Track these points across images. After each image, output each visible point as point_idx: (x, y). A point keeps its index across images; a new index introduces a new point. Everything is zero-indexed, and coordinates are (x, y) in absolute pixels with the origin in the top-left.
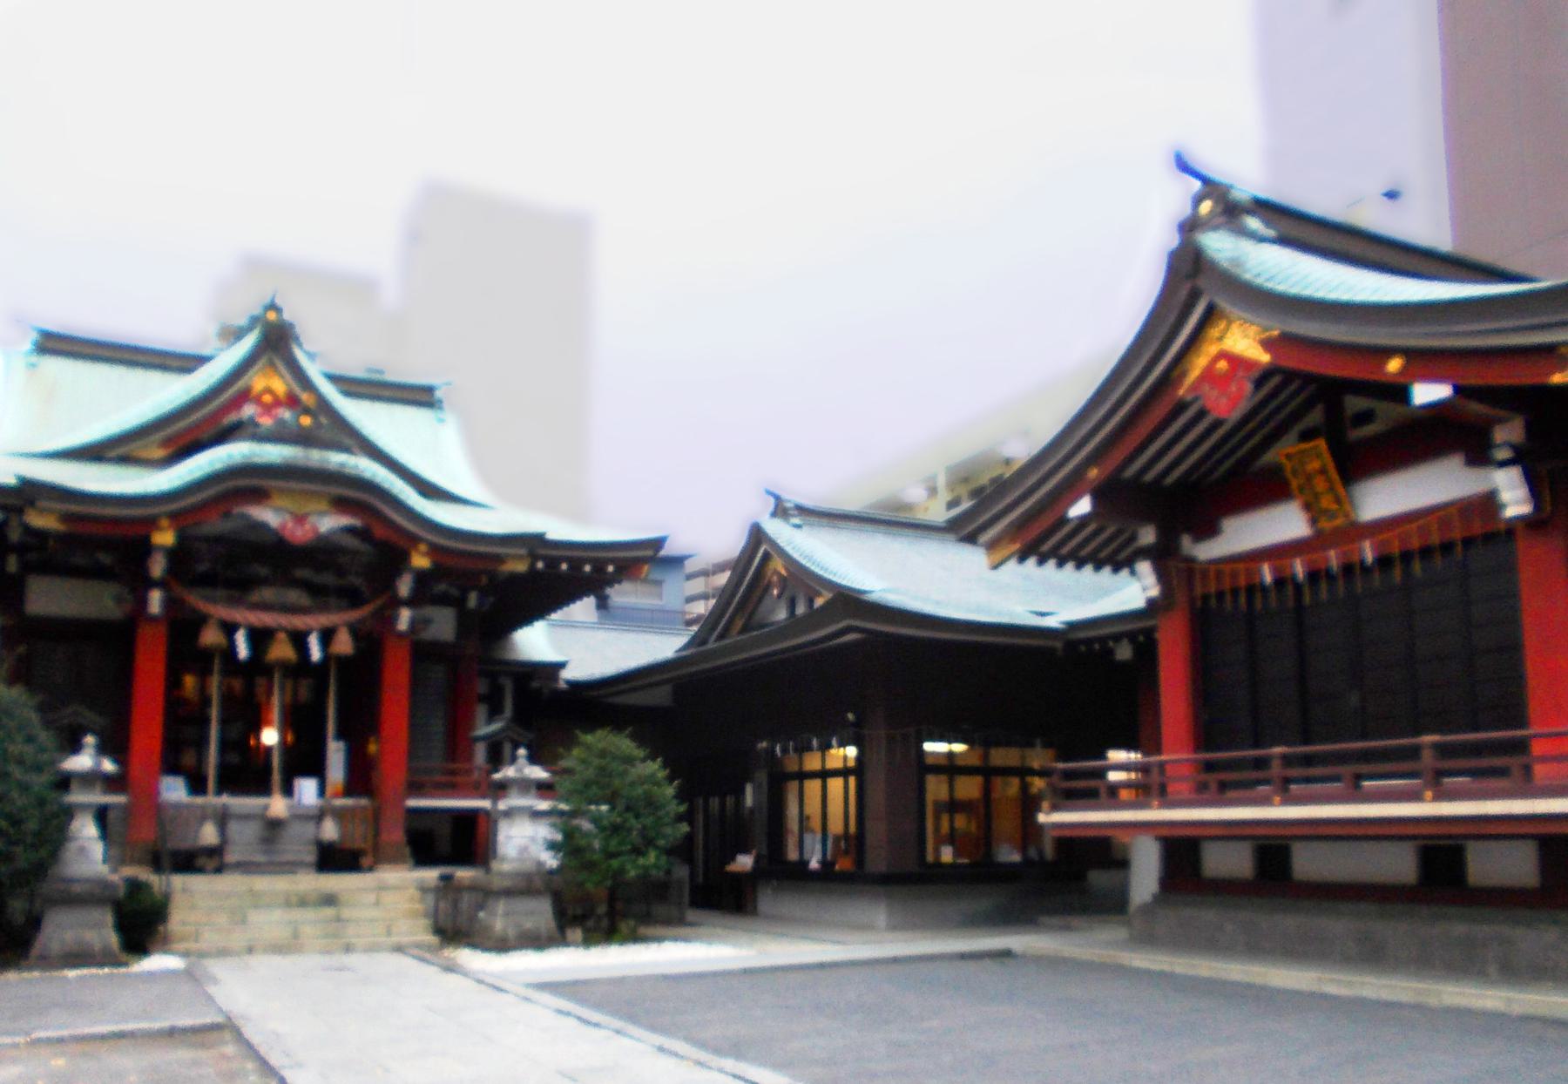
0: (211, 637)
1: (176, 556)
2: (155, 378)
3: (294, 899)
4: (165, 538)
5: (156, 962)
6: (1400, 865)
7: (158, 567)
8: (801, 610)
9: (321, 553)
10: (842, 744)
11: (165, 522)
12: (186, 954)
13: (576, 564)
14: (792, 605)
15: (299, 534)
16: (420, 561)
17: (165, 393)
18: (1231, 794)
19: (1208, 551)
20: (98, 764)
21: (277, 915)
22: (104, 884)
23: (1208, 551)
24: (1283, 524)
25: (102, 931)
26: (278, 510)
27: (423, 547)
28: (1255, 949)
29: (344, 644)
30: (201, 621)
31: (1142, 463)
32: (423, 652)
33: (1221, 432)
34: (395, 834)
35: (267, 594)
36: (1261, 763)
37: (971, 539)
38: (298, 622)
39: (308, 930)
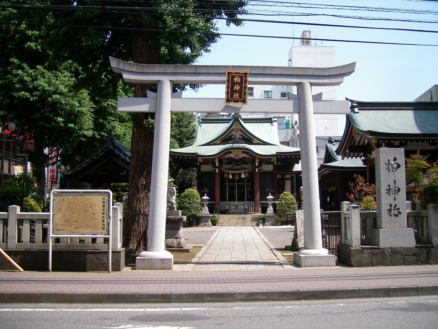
0: (226, 176)
29: (247, 175)
38: (239, 172)
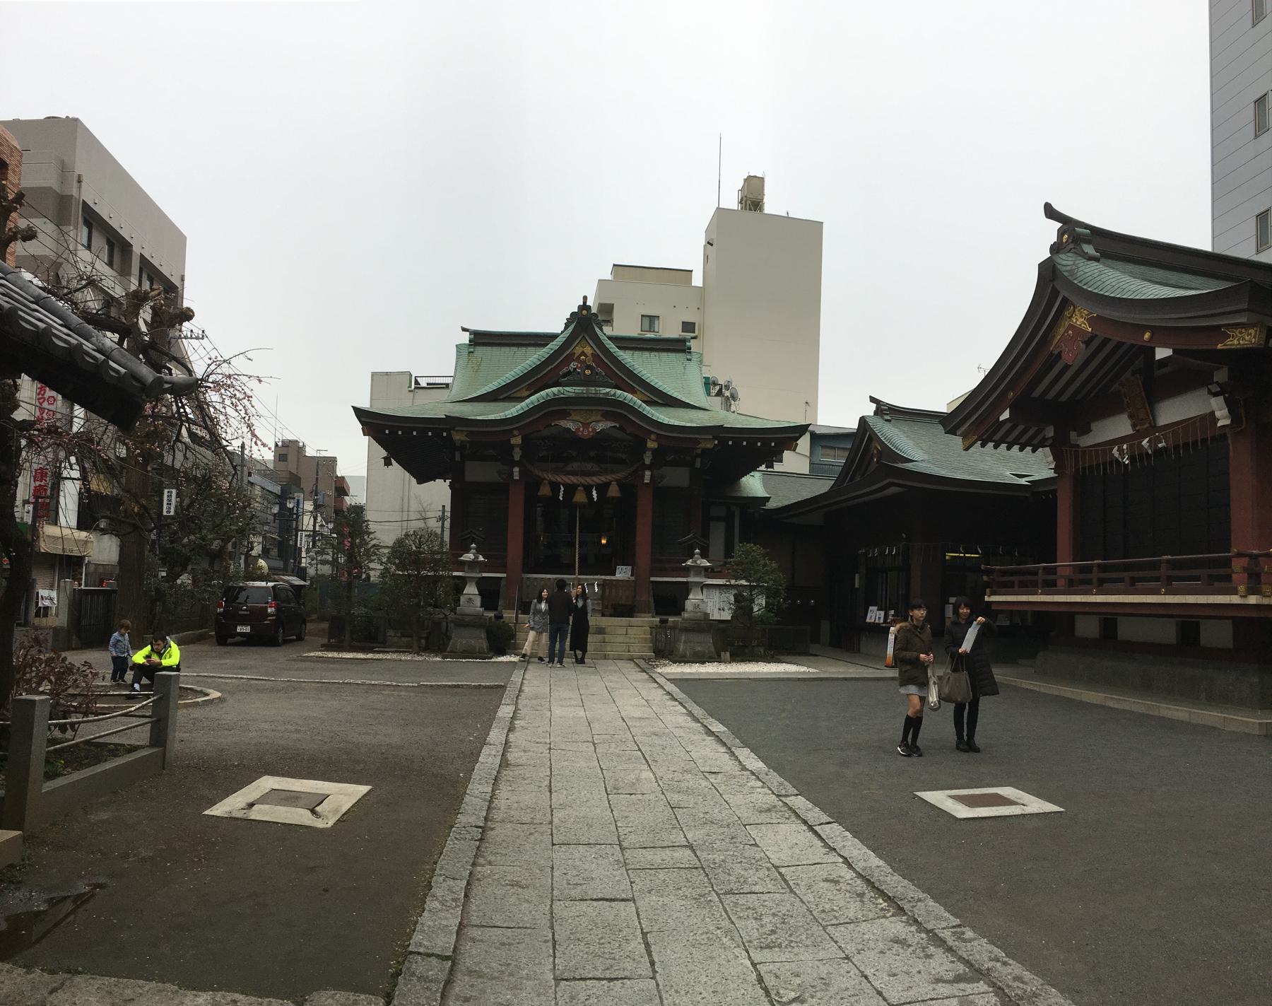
0: (545, 490)
1: (525, 446)
2: (522, 351)
4: (517, 440)
6: (1167, 633)
7: (517, 455)
9: (600, 440)
13: (752, 442)
15: (586, 433)
16: (652, 444)
17: (534, 357)
18: (1139, 585)
19: (1087, 441)
22: (480, 617)
23: (1087, 441)
24: (1120, 427)
25: (481, 642)
26: (574, 421)
27: (653, 437)
28: (1093, 681)
29: (614, 491)
30: (538, 483)
31: (1021, 393)
32: (662, 495)
33: (1068, 375)
34: (646, 598)
35: (575, 466)
36: (1155, 566)
37: (952, 431)
38: (589, 480)
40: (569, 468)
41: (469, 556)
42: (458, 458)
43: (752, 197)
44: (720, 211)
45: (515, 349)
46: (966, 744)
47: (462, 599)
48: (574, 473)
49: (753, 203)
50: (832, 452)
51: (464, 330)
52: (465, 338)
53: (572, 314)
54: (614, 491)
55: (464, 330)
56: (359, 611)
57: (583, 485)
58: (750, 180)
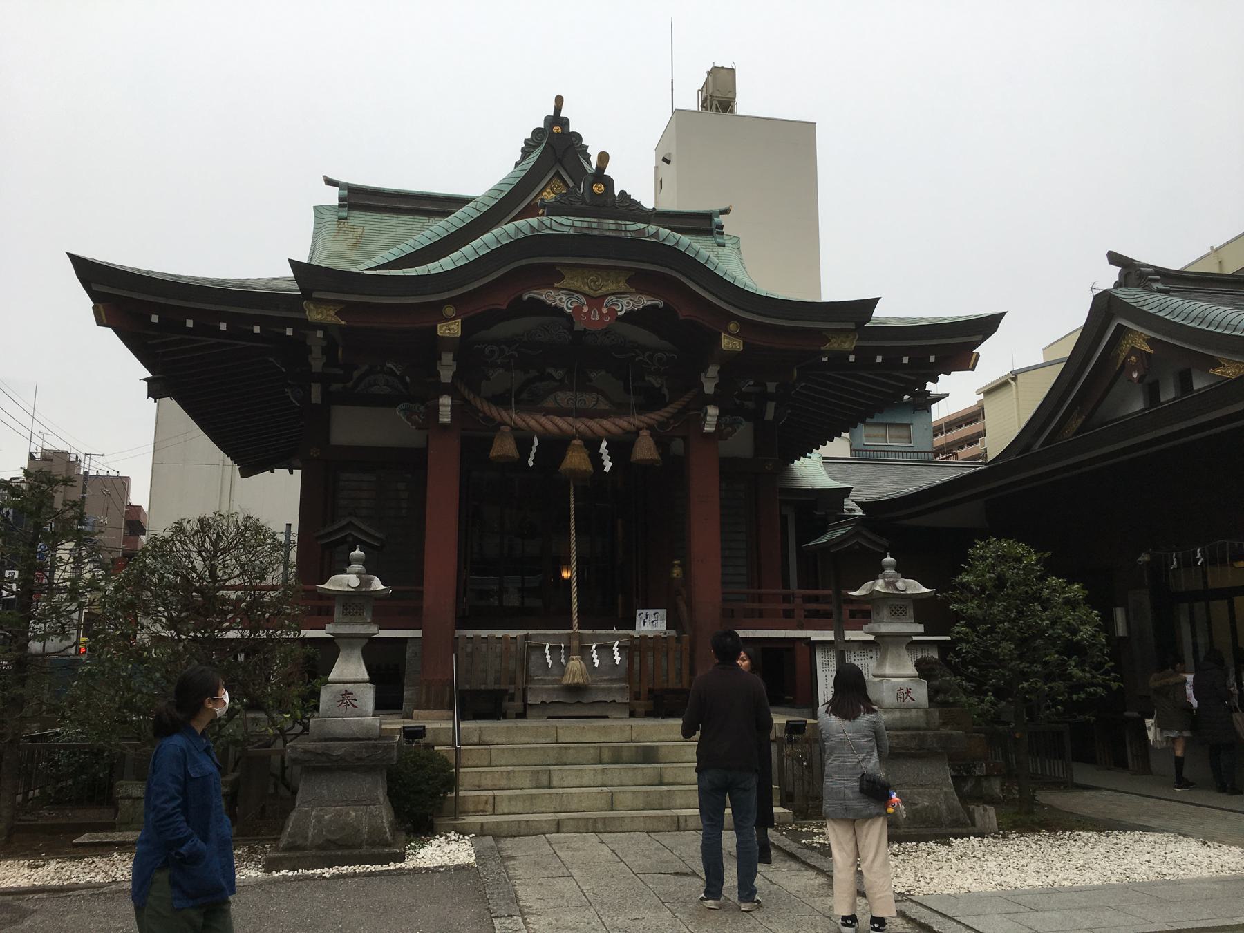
0: (505, 447)
3: (606, 756)
4: (451, 329)
5: (444, 852)
8: (1168, 394)
10: (44, 654)
11: (449, 311)
12: (481, 832)
14: (1153, 393)
15: (594, 318)
20: (365, 583)
21: (589, 772)
27: (732, 327)
29: (645, 449)
35: (563, 398)
39: (625, 796)
40: (549, 403)
41: (347, 581)
42: (316, 395)
43: (719, 93)
44: (677, 113)
45: (424, 219)
46: (817, 798)
47: (326, 696)
48: (563, 413)
49: (721, 103)
50: (894, 432)
51: (329, 182)
52: (332, 197)
53: (536, 132)
54: (645, 449)
55: (329, 182)
56: (67, 731)
57: (582, 437)
58: (715, 72)
